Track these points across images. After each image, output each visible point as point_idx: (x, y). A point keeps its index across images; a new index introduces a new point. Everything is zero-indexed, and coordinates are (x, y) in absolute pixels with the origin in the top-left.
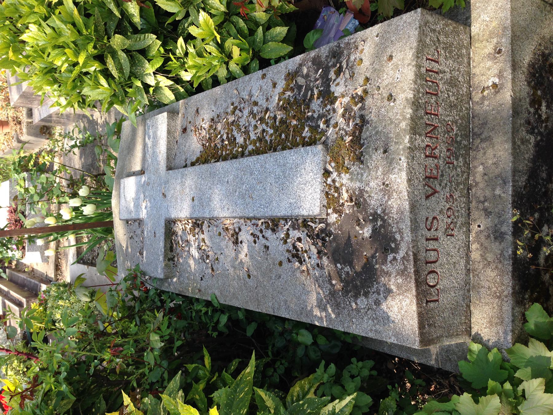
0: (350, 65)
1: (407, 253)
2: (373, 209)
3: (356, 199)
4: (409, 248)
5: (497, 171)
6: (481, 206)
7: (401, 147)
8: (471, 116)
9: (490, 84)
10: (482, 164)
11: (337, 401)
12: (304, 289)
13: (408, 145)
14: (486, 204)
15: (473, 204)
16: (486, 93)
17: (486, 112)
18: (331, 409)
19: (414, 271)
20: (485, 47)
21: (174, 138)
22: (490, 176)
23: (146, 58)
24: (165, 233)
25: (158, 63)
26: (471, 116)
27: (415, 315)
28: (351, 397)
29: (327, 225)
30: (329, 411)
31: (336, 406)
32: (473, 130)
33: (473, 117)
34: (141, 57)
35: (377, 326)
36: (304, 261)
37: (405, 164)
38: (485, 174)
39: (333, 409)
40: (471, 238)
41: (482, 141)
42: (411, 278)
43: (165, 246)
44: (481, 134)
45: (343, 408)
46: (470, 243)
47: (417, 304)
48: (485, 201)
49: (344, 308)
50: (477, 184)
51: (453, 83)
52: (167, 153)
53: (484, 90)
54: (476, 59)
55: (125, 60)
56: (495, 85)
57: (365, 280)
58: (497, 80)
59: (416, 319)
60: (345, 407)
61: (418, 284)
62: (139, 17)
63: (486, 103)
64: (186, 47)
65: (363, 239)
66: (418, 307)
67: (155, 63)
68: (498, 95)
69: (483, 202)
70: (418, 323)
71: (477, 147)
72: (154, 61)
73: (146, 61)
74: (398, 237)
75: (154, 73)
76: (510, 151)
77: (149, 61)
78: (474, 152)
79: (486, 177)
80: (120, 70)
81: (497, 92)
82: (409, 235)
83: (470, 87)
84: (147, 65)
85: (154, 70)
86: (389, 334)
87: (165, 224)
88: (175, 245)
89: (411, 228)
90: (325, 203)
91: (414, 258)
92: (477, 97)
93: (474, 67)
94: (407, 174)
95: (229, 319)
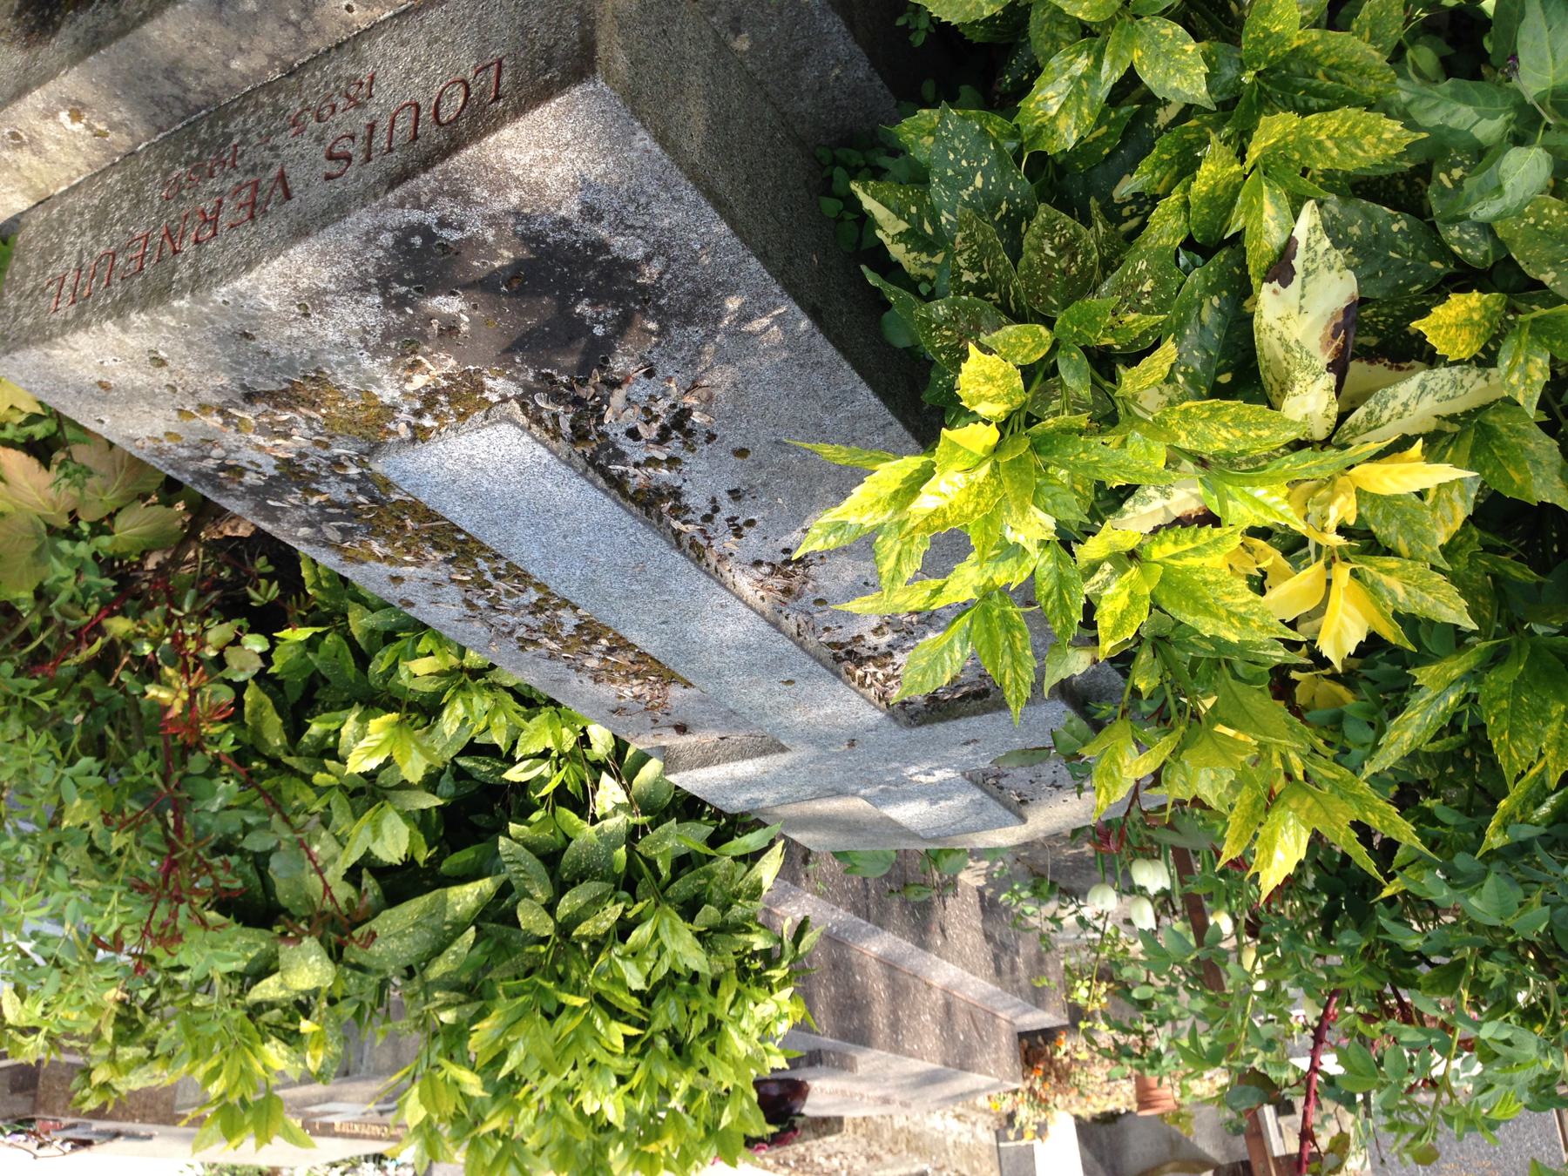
0: (198, 453)
1: (401, 205)
2: (383, 314)
3: (404, 355)
4: (384, 206)
5: (214, 28)
6: (307, 26)
7: (205, 310)
8: (161, 135)
9: (78, 127)
10: (227, 66)
11: (879, 234)
12: (749, 382)
13: (188, 296)
14: (294, 17)
15: (317, 44)
16: (102, 127)
17: (131, 109)
18: (902, 246)
19: (425, 171)
20: (30, 166)
21: (716, 746)
22: (234, 37)
23: (564, 850)
24: (941, 720)
25: (568, 816)
26: (161, 135)
27: (522, 123)
28: (861, 195)
29: (529, 391)
30: (908, 251)
31: (892, 233)
32: (183, 119)
33: (160, 129)
34: (566, 859)
35: (651, 190)
36: (673, 406)
37: (224, 290)
38: (240, 49)
39: (900, 241)
40: (387, 14)
41: (187, 90)
42: (445, 172)
43: (975, 713)
44: (177, 98)
45: (892, 211)
46: (398, 10)
47: (496, 130)
48: (288, 22)
49: (693, 279)
50: (272, 57)
51: (100, 220)
52: (751, 757)
53: (103, 135)
54: (64, 175)
55: (576, 896)
56: (76, 116)
57: (567, 263)
58: (64, 116)
59: (530, 116)
60: (887, 206)
61: (455, 146)
62: (480, 883)
63: (116, 117)
64: (522, 760)
65: (475, 307)
66: (503, 124)
67: (571, 824)
68: (84, 100)
69: (296, 25)
70: (538, 106)
71: (204, 92)
72: (566, 828)
73: (572, 845)
74: (386, 239)
75: (594, 821)
76: (158, 22)
77: (569, 840)
78: (219, 93)
79: (244, 45)
80: (597, 903)
81: (84, 106)
82: (354, 219)
83: (114, 164)
84: (579, 840)
85: (586, 825)
86: (639, 158)
87: (919, 725)
88: (965, 689)
89: (340, 218)
90: (479, 415)
91: (399, 183)
92: (121, 141)
93: (79, 174)
94: (237, 278)
95: (131, 797)
